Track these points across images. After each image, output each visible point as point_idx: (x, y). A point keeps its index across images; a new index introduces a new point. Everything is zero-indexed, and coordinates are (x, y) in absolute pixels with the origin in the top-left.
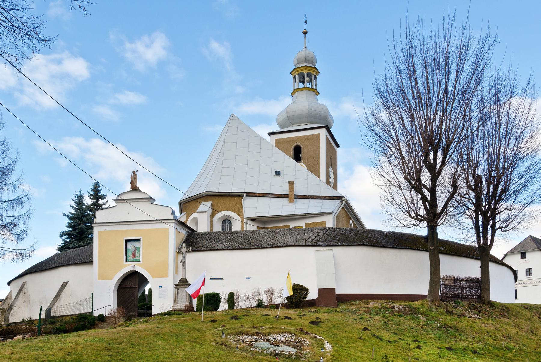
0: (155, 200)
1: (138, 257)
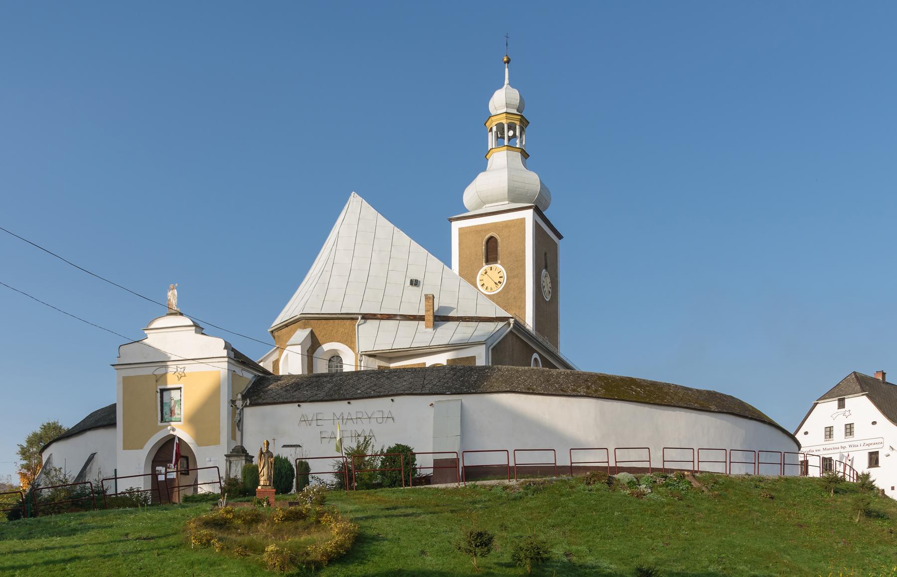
0: (203, 329)
1: (178, 414)
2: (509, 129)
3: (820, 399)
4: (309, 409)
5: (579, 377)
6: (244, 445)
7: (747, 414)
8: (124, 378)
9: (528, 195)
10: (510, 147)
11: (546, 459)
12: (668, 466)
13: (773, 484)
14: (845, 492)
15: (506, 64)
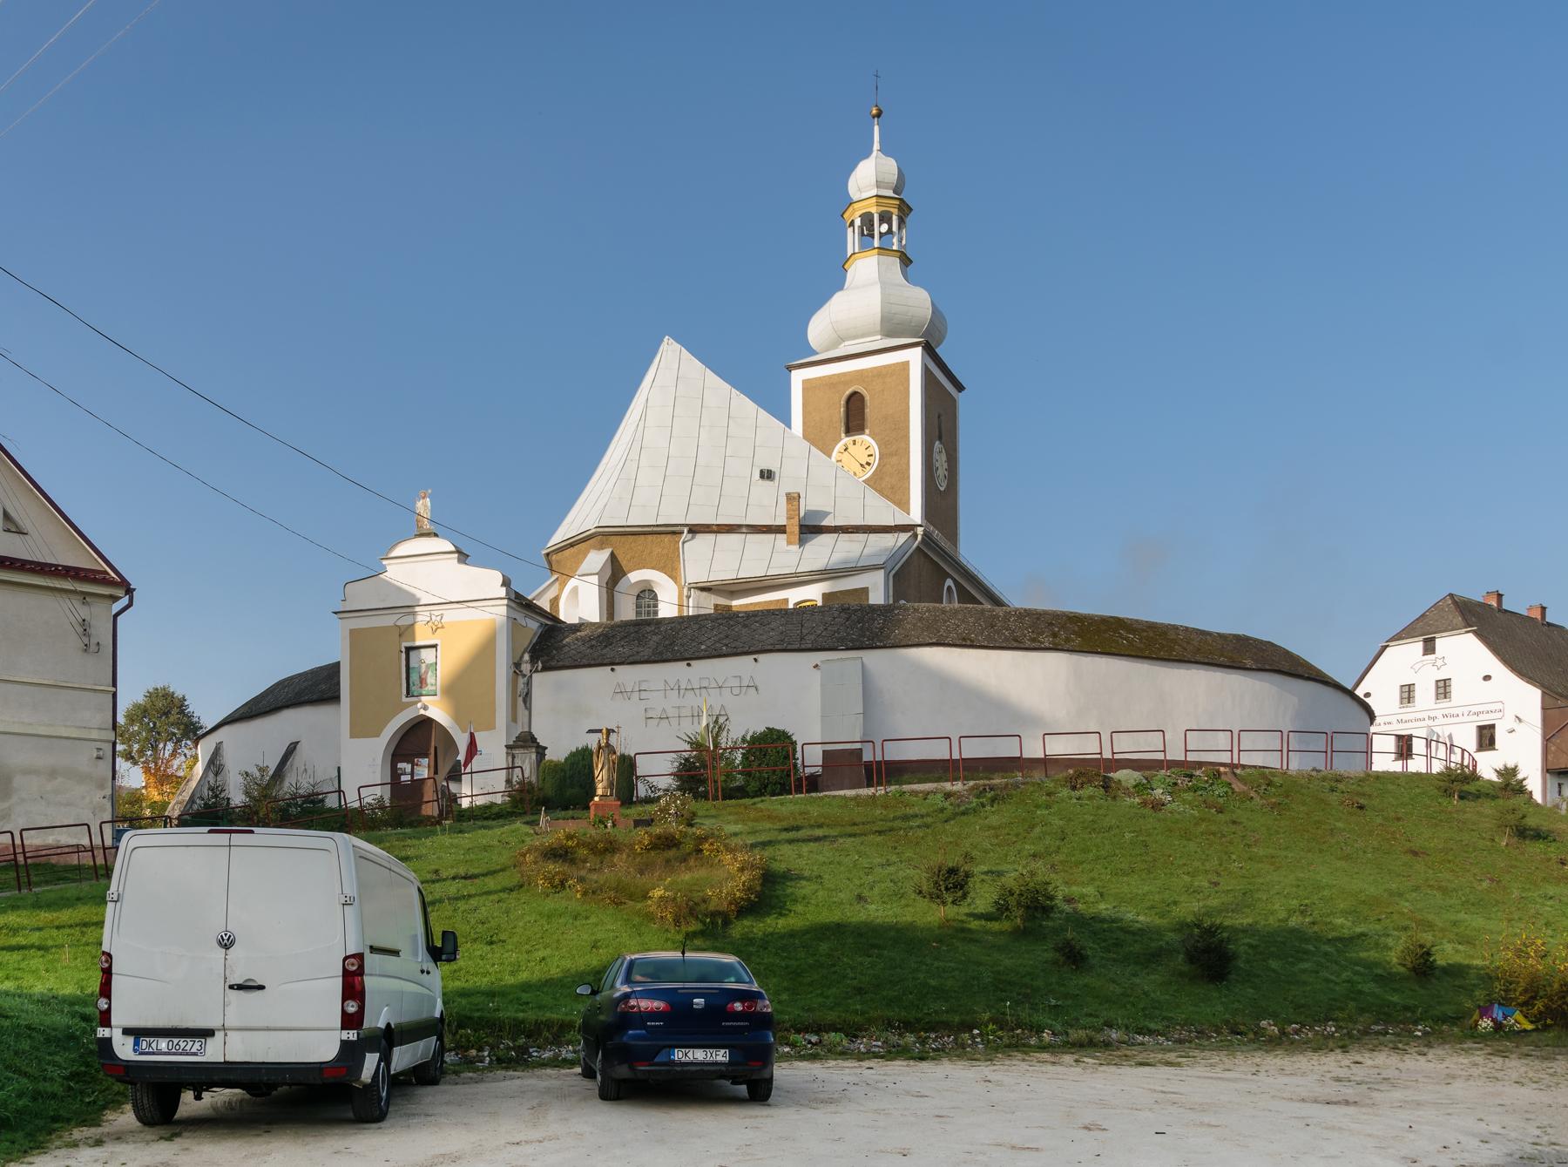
0: (468, 556)
1: (432, 685)
2: (882, 221)
3: (1392, 639)
4: (628, 674)
5: (1038, 619)
6: (534, 731)
7: (1300, 671)
8: (352, 632)
9: (913, 324)
10: (883, 250)
11: (1007, 749)
12: (1192, 757)
13: (1359, 785)
14: (1478, 796)
15: (876, 119)
